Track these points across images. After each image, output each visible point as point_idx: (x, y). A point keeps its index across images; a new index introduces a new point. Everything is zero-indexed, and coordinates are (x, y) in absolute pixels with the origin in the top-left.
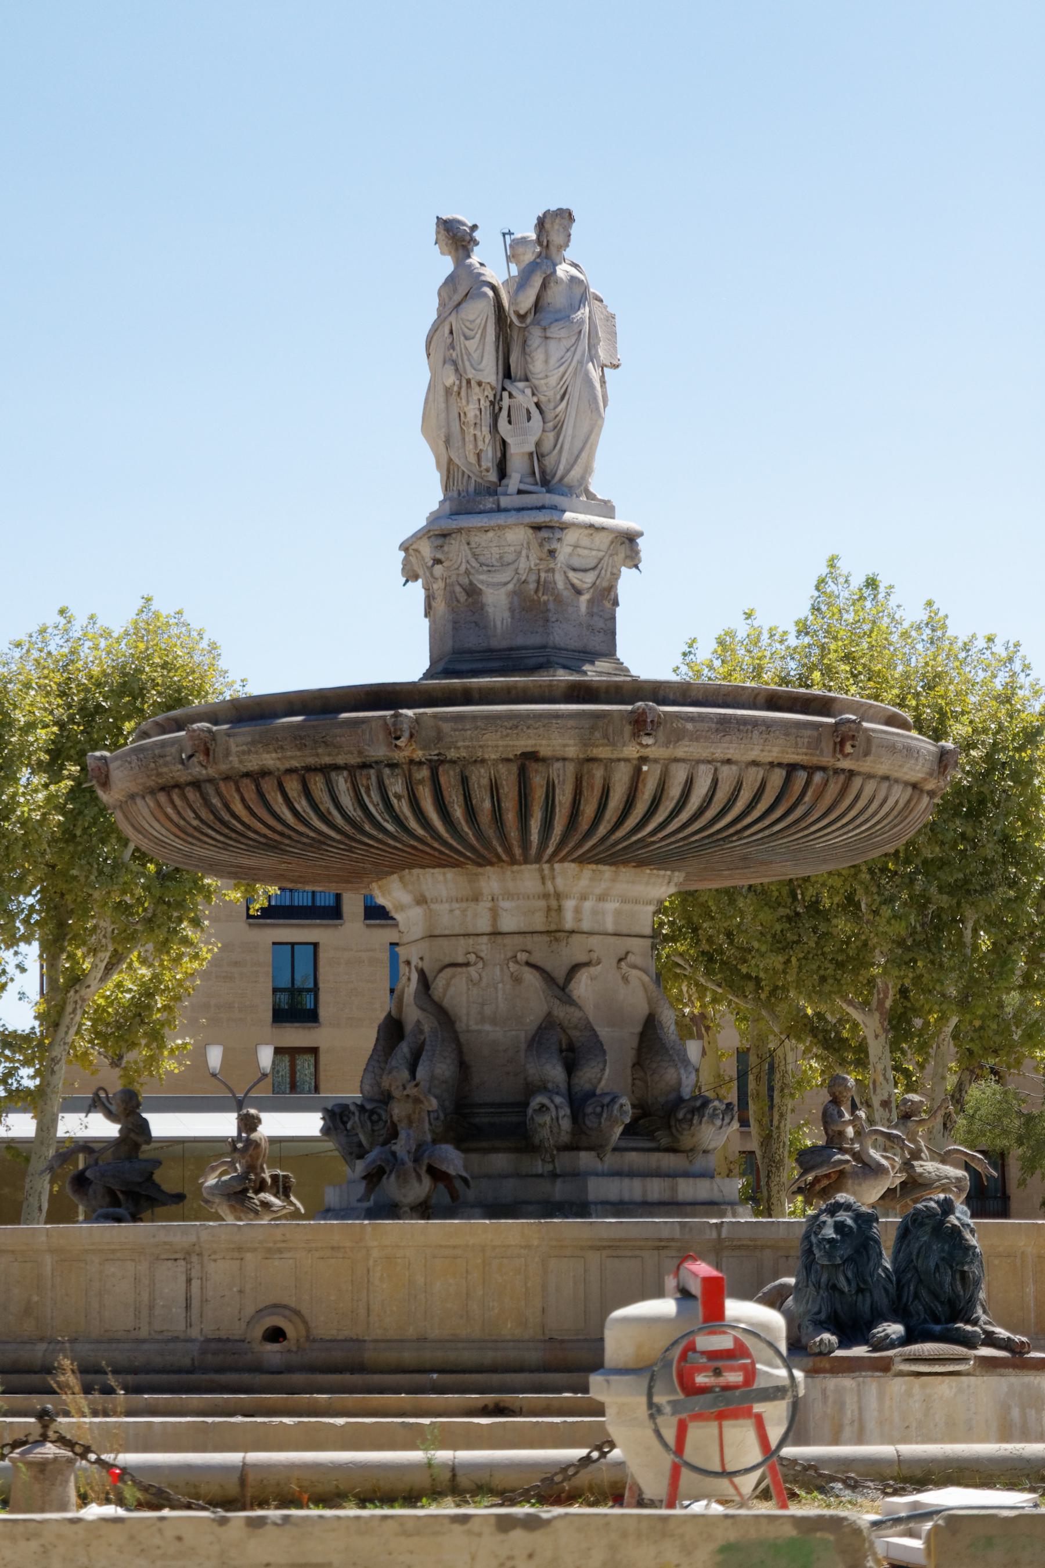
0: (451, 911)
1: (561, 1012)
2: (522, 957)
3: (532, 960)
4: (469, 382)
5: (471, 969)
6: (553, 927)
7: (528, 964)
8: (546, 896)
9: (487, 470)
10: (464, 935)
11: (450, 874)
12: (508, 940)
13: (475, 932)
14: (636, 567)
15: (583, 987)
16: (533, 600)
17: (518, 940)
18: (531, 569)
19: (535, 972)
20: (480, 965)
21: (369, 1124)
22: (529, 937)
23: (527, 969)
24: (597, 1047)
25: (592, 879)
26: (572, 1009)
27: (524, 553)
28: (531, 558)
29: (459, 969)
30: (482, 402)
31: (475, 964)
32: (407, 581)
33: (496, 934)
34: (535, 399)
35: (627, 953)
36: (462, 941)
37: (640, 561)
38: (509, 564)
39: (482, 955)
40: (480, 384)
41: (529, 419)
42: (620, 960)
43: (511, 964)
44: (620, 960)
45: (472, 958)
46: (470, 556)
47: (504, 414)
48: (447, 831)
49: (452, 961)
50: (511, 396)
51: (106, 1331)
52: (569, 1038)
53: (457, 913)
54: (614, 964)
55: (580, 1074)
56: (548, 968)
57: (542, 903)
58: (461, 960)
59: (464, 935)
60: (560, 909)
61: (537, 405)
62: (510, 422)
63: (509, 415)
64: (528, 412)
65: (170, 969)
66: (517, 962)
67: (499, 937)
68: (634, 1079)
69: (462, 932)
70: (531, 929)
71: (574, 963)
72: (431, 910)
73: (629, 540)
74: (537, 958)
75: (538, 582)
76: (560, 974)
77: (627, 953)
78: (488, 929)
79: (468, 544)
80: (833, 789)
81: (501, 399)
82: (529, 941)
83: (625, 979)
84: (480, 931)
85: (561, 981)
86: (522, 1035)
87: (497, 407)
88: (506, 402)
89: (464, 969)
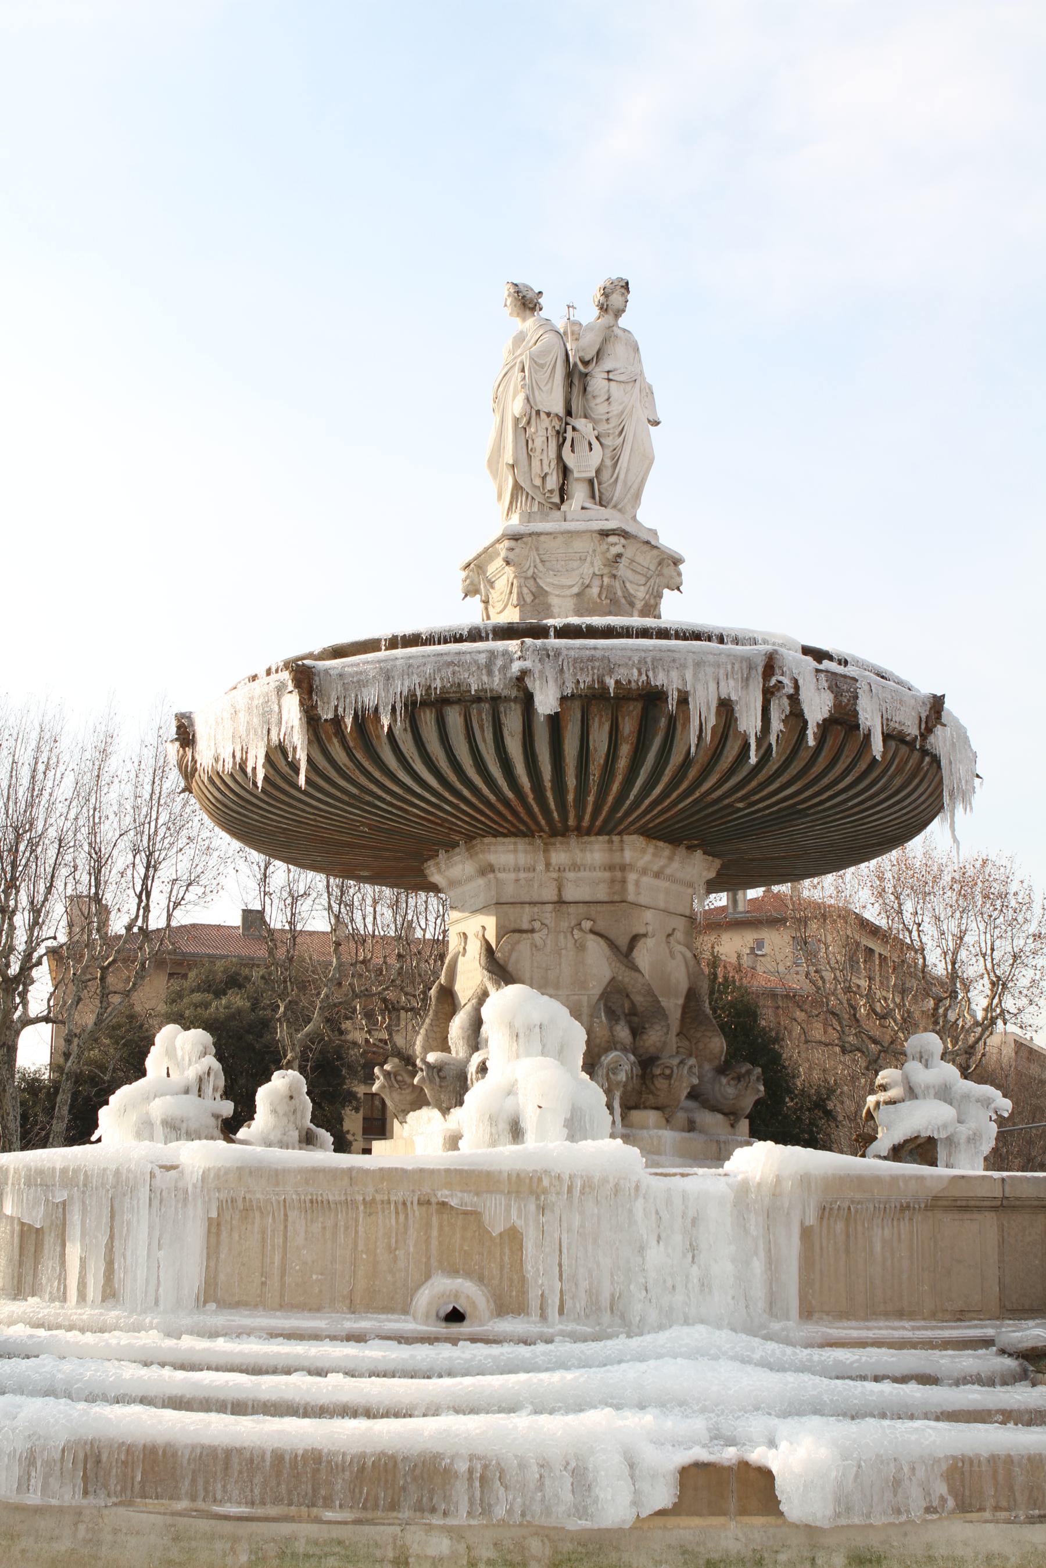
0: (517, 880)
1: (626, 977)
2: (587, 925)
3: (596, 929)
4: (538, 412)
5: (536, 936)
6: (616, 898)
7: (592, 931)
8: (611, 868)
9: (551, 491)
10: (530, 903)
11: (521, 844)
12: (572, 909)
13: (540, 900)
14: (678, 589)
15: (643, 956)
16: (596, 603)
17: (582, 909)
18: (594, 574)
19: (600, 939)
20: (545, 931)
21: (437, 1079)
22: (593, 907)
23: (592, 936)
24: (659, 1012)
25: (654, 855)
26: (637, 975)
27: (589, 559)
28: (596, 564)
29: (524, 935)
30: (549, 431)
31: (540, 931)
32: (466, 596)
33: (561, 902)
34: (596, 432)
35: (674, 930)
36: (527, 908)
37: (681, 584)
38: (573, 570)
39: (547, 922)
40: (548, 414)
41: (591, 449)
42: (669, 935)
43: (575, 932)
44: (669, 935)
45: (537, 925)
46: (538, 561)
47: (568, 443)
48: (552, 781)
49: (517, 927)
50: (574, 429)
51: (226, 1426)
52: (632, 1002)
53: (522, 882)
54: (664, 938)
55: (645, 1037)
56: (612, 937)
57: (607, 875)
58: (525, 926)
59: (530, 903)
60: (624, 881)
61: (597, 438)
62: (573, 451)
63: (572, 445)
64: (590, 444)
65: (604, 553)
66: (581, 929)
67: (565, 906)
68: (678, 1047)
69: (527, 900)
70: (594, 899)
71: (634, 933)
72: (497, 879)
73: (677, 561)
74: (601, 926)
75: (601, 587)
76: (623, 942)
77: (674, 930)
78: (555, 898)
79: (537, 549)
80: (628, 726)
81: (565, 432)
82: (593, 910)
83: (672, 955)
84: (545, 899)
85: (624, 949)
86: (585, 999)
87: (561, 439)
88: (569, 434)
89: (530, 935)
